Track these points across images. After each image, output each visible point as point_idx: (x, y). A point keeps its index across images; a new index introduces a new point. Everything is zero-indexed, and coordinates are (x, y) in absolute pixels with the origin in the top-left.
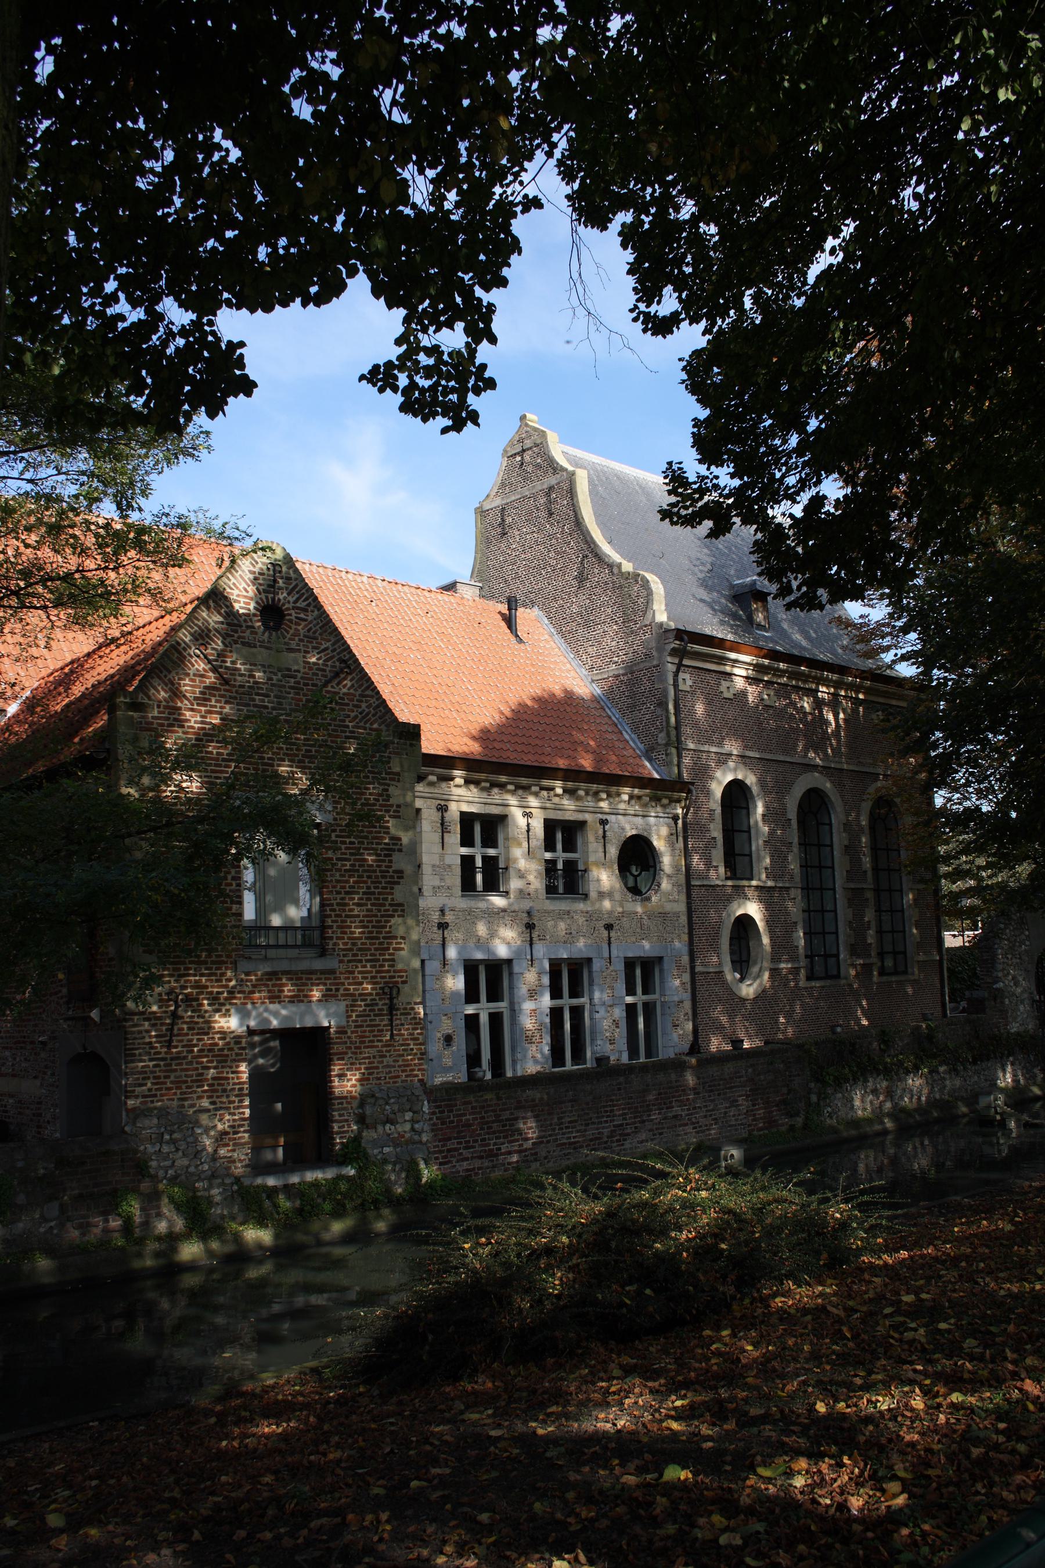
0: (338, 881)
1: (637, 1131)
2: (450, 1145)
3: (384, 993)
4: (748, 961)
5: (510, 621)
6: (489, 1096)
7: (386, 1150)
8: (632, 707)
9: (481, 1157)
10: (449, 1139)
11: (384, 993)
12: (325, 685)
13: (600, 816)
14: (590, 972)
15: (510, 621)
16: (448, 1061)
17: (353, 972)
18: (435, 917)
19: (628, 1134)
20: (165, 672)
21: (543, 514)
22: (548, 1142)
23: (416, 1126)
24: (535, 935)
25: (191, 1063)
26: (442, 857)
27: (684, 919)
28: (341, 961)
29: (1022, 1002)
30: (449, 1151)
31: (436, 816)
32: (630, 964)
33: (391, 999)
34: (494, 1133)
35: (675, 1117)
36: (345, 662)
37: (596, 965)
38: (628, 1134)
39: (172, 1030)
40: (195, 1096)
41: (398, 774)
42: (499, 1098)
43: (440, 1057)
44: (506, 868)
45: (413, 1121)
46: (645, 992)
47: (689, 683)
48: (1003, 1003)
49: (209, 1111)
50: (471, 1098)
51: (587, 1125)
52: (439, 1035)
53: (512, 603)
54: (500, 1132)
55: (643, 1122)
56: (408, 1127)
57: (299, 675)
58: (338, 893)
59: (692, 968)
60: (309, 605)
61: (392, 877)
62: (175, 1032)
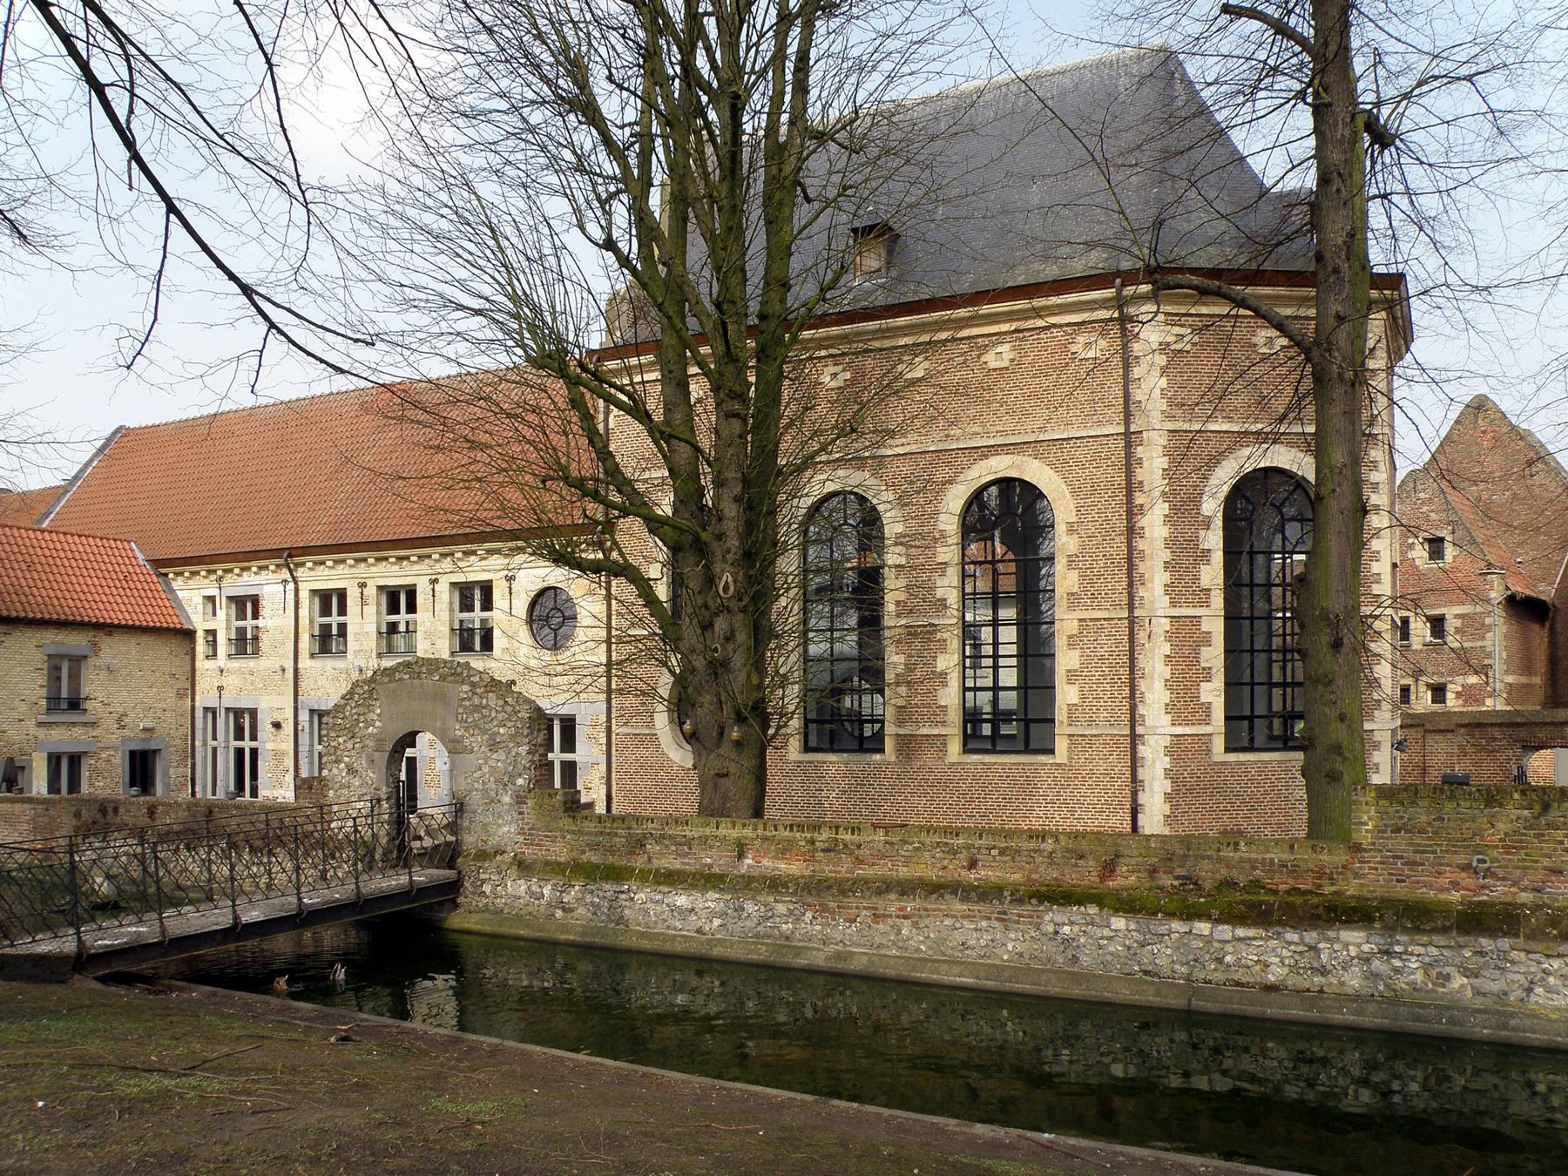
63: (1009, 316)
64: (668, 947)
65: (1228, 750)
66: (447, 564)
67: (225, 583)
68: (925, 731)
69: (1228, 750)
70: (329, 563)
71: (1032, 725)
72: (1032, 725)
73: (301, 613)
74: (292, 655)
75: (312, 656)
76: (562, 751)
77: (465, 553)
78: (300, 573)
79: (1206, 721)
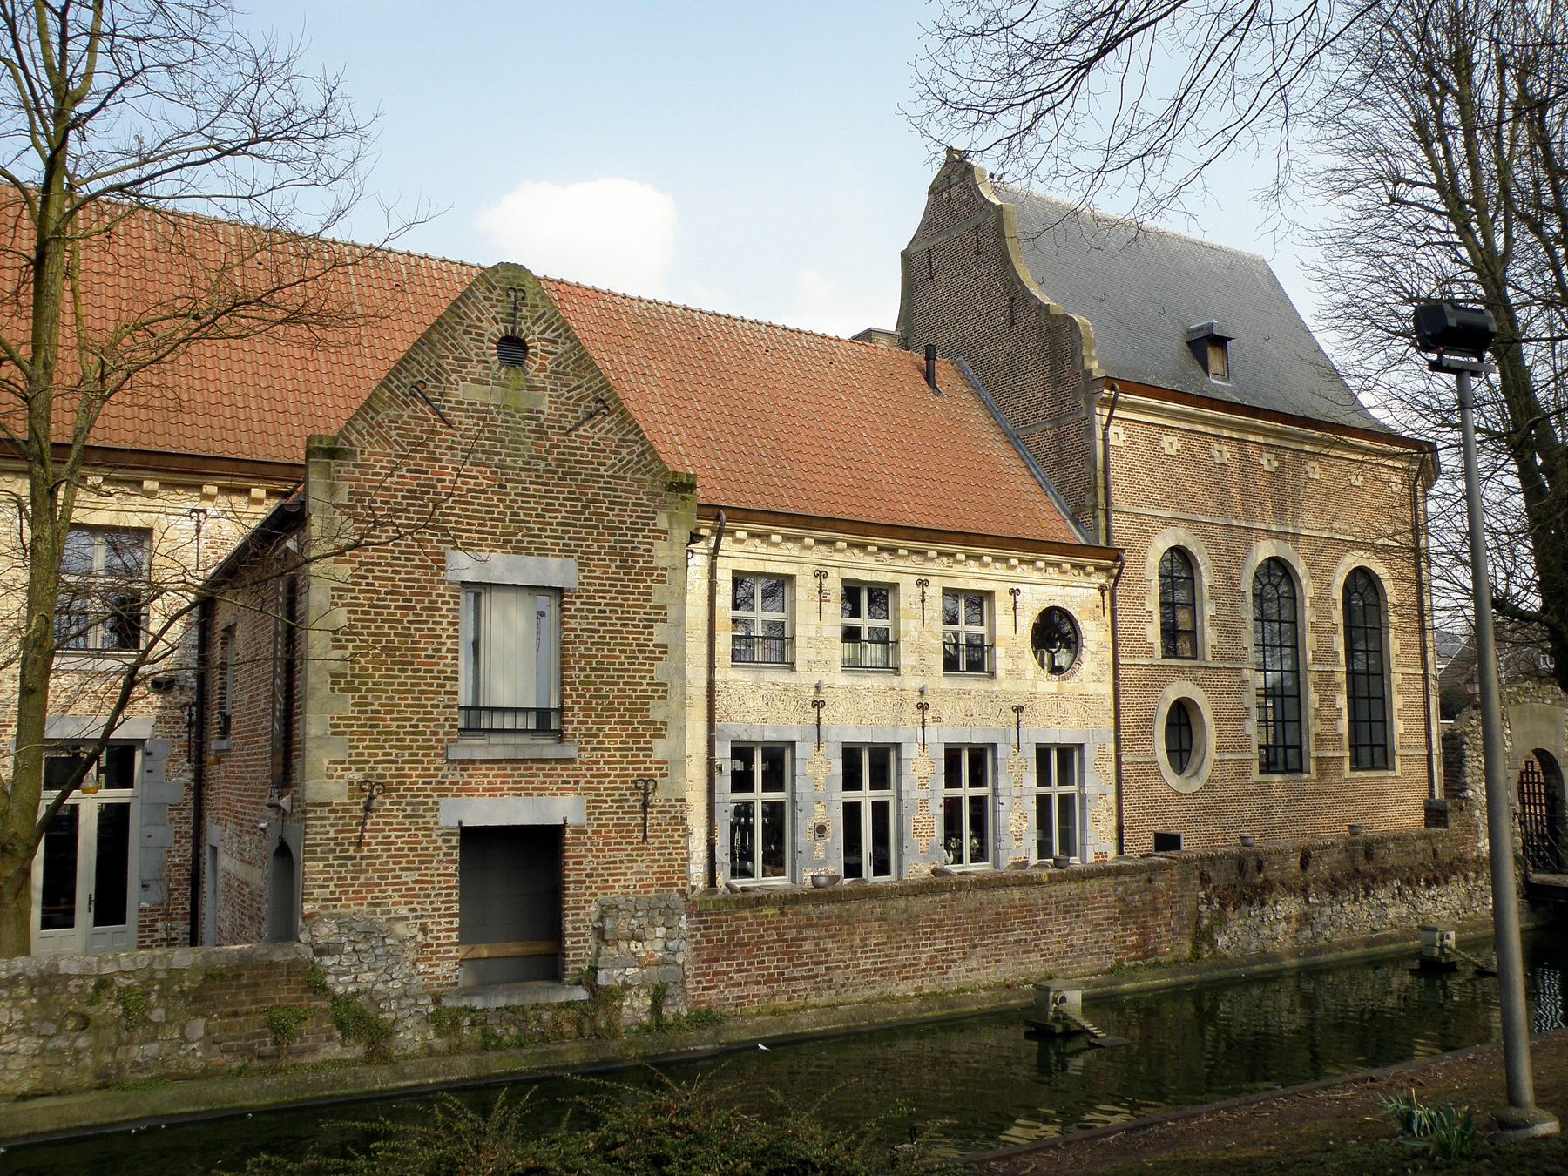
0: (581, 656)
1: (966, 957)
2: (717, 967)
3: (638, 788)
4: (1189, 751)
5: (929, 376)
6: (770, 911)
7: (630, 971)
8: (1060, 464)
9: (758, 983)
11: (638, 788)
12: (575, 428)
13: (1010, 585)
14: (995, 759)
15: (929, 376)
16: (820, 854)
17: (598, 762)
18: (810, 695)
19: (953, 961)
20: (372, 414)
21: (971, 253)
22: (847, 967)
23: (670, 944)
24: (928, 717)
25: (387, 863)
26: (819, 629)
27: (1110, 702)
28: (581, 749)
30: (715, 974)
31: (917, 591)
32: (1043, 753)
33: (646, 795)
35: (1017, 942)
36: (603, 401)
38: (953, 961)
39: (364, 824)
40: (390, 901)
41: (665, 532)
42: (783, 914)
43: (811, 849)
44: (897, 642)
45: (667, 938)
46: (1062, 782)
47: (1123, 437)
48: (1472, 816)
49: (407, 918)
50: (747, 913)
51: (899, 948)
52: (811, 825)
53: (930, 354)
56: (659, 945)
57: (543, 417)
58: (582, 669)
59: (1118, 758)
60: (559, 336)
61: (652, 652)
62: (368, 827)
63: (1366, 451)
65: (1261, 772)
68: (1330, 754)
70: (1041, 564)
74: (704, 660)
76: (765, 789)
77: (881, 549)
79: (1340, 748)
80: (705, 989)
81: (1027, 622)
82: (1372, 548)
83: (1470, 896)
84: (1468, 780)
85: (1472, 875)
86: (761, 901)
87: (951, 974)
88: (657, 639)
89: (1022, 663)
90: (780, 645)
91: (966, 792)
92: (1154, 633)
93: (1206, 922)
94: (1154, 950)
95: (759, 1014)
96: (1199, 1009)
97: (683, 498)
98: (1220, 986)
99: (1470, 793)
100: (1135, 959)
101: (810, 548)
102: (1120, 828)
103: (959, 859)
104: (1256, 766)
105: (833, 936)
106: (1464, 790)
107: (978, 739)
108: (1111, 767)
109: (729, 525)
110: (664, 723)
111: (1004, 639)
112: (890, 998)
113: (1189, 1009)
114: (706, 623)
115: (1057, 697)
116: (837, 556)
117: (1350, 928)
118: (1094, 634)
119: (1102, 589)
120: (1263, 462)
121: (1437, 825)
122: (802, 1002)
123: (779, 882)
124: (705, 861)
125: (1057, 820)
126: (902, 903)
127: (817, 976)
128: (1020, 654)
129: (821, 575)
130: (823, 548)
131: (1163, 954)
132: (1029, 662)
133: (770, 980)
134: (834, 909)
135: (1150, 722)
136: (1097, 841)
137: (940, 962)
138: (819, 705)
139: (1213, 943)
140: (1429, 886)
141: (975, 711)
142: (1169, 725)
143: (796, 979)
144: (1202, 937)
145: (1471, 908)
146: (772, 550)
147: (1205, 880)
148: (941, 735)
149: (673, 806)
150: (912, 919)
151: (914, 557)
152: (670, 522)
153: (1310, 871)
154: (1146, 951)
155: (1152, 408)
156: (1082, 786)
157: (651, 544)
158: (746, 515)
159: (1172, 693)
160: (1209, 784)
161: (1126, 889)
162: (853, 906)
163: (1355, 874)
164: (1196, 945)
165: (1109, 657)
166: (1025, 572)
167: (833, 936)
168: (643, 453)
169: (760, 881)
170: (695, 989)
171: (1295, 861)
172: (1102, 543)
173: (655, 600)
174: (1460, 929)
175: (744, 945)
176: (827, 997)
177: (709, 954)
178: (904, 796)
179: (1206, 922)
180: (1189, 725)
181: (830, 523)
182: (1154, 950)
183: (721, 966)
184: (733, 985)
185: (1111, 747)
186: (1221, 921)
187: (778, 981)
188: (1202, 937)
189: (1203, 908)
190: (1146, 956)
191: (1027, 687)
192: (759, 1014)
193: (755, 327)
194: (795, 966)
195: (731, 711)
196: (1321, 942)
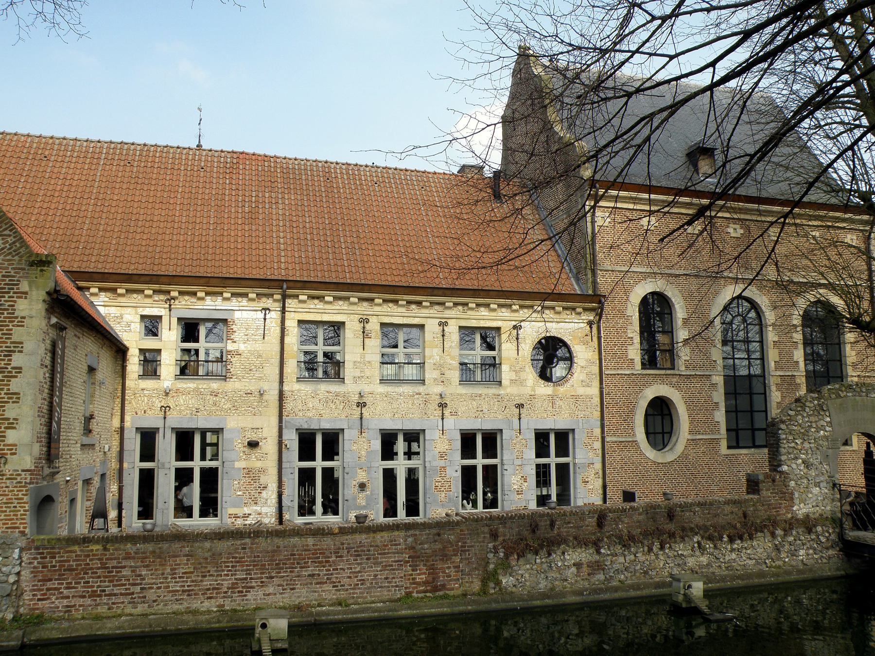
1: (263, 585)
2: (49, 585)
6: (95, 547)
9: (84, 597)
10: (50, 580)
13: (514, 323)
18: (355, 398)
22: (159, 588)
24: (447, 412)
26: (363, 356)
27: (597, 400)
29: (817, 484)
30: (48, 589)
31: (359, 327)
34: (99, 577)
37: (506, 435)
41: (26, 293)
42: (105, 549)
43: (355, 499)
44: (500, 364)
50: (76, 548)
51: (205, 576)
54: (106, 577)
55: (272, 578)
59: (603, 438)
64: (787, 578)
65: (729, 447)
66: (457, 312)
67: (176, 304)
69: (729, 447)
71: (756, 432)
72: (756, 432)
73: (287, 340)
75: (299, 380)
76: (314, 460)
78: (291, 303)
80: (39, 600)
81: (527, 348)
82: (831, 286)
83: (777, 549)
84: (783, 458)
85: (779, 532)
86: (320, 532)
87: (249, 596)
88: (14, 364)
89: (523, 375)
90: (333, 367)
91: (553, 460)
92: (635, 353)
93: (492, 566)
94: (443, 586)
95: (83, 618)
96: (486, 631)
97: (42, 271)
98: (505, 616)
99: (785, 468)
100: (425, 592)
101: (355, 304)
102: (604, 487)
103: (475, 505)
104: (724, 444)
105: (147, 566)
106: (780, 465)
107: (488, 426)
108: (598, 445)
109: (290, 292)
110: (16, 419)
111: (509, 359)
112: (195, 612)
113: (478, 630)
114: (279, 354)
115: (552, 398)
116: (377, 308)
117: (646, 573)
118: (584, 354)
119: (590, 323)
120: (731, 230)
121: (754, 493)
122: (119, 611)
123: (210, 523)
124: (277, 505)
125: (554, 478)
126: (207, 545)
127: (133, 593)
128: (522, 369)
129: (364, 321)
130: (365, 304)
131: (452, 589)
132: (531, 376)
133: (93, 595)
134: (150, 547)
135: (632, 412)
136: (586, 492)
137: (241, 588)
138: (361, 405)
139: (498, 583)
140: (731, 540)
141: (485, 407)
142: (647, 415)
143: (115, 595)
144: (489, 578)
145: (779, 559)
146: (328, 306)
147: (494, 536)
148: (455, 425)
149: (20, 475)
150: (215, 556)
151: (437, 307)
152: (30, 286)
153: (606, 528)
154: (434, 586)
155: (631, 198)
156: (574, 458)
157: (15, 302)
158: (128, 278)
159: (651, 393)
160: (684, 456)
161: (415, 541)
162: (165, 546)
163: (657, 533)
164: (484, 582)
165: (596, 369)
166: (524, 313)
167: (147, 566)
168: (14, 242)
169: (319, 518)
170: (31, 600)
171: (592, 521)
172: (590, 292)
173: (15, 338)
174: (707, 580)
175: (74, 570)
176: (140, 609)
177: (43, 578)
178: (427, 465)
179: (492, 566)
180: (670, 415)
181: (366, 288)
182: (443, 586)
183: (54, 584)
184: (62, 598)
185: (598, 431)
186: (505, 565)
187: (100, 596)
188: (489, 578)
189: (491, 556)
190: (435, 589)
191: (528, 391)
192: (83, 618)
193: (284, 161)
194: (114, 586)
195: (296, 410)
196: (615, 583)
